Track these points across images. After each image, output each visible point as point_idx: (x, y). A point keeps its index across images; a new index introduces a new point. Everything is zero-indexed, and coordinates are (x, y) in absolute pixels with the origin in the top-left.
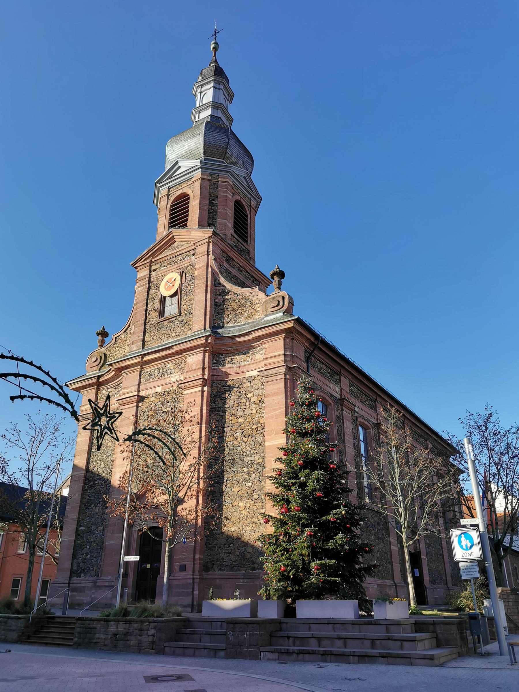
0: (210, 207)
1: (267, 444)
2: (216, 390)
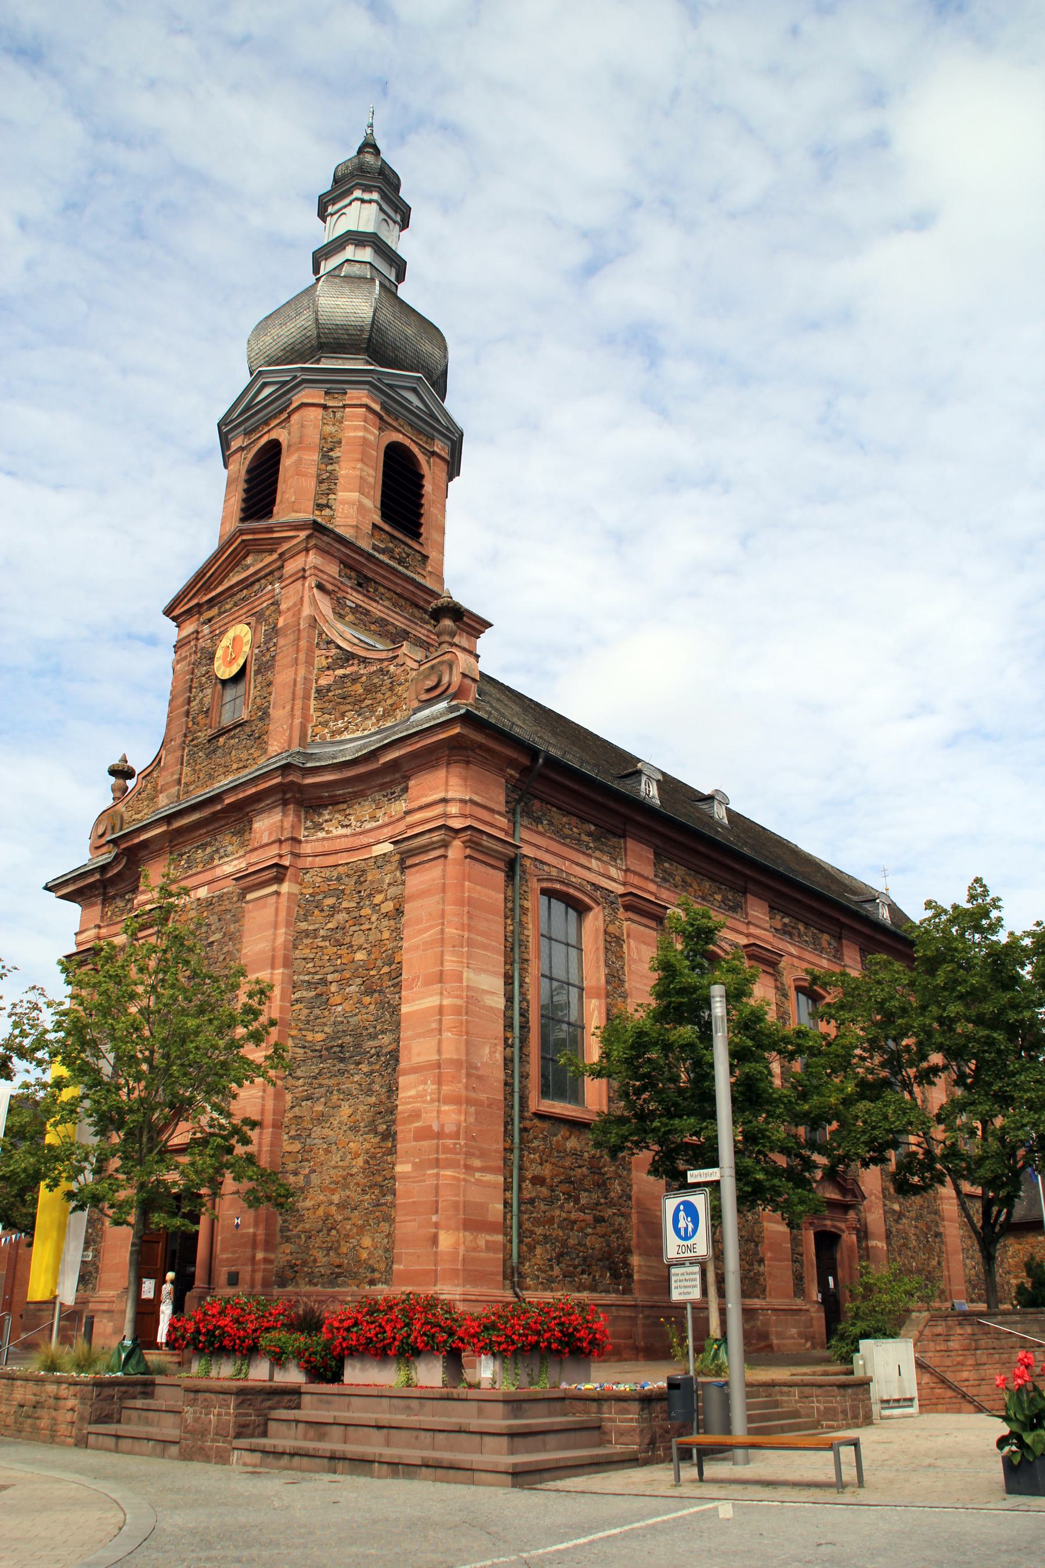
0: (323, 467)
1: (405, 1009)
2: (311, 891)
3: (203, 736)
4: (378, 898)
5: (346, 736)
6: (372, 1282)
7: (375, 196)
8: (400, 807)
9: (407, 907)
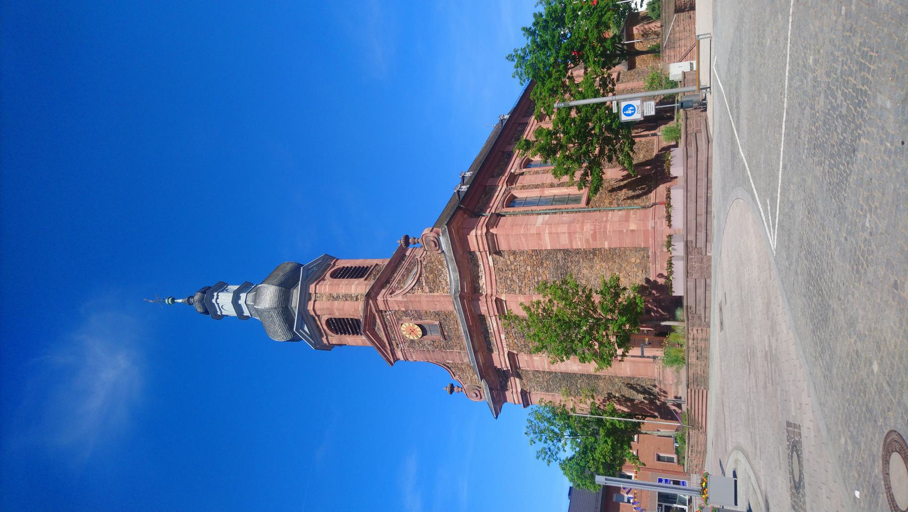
1: (549, 248)
3: (443, 343)
4: (509, 262)
5: (448, 280)
6: (648, 257)
7: (215, 294)
8: (478, 253)
9: (513, 249)
